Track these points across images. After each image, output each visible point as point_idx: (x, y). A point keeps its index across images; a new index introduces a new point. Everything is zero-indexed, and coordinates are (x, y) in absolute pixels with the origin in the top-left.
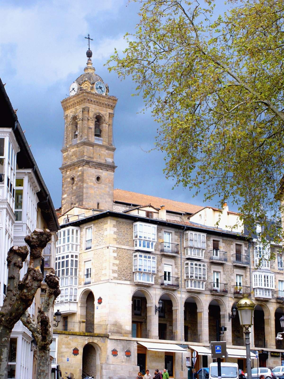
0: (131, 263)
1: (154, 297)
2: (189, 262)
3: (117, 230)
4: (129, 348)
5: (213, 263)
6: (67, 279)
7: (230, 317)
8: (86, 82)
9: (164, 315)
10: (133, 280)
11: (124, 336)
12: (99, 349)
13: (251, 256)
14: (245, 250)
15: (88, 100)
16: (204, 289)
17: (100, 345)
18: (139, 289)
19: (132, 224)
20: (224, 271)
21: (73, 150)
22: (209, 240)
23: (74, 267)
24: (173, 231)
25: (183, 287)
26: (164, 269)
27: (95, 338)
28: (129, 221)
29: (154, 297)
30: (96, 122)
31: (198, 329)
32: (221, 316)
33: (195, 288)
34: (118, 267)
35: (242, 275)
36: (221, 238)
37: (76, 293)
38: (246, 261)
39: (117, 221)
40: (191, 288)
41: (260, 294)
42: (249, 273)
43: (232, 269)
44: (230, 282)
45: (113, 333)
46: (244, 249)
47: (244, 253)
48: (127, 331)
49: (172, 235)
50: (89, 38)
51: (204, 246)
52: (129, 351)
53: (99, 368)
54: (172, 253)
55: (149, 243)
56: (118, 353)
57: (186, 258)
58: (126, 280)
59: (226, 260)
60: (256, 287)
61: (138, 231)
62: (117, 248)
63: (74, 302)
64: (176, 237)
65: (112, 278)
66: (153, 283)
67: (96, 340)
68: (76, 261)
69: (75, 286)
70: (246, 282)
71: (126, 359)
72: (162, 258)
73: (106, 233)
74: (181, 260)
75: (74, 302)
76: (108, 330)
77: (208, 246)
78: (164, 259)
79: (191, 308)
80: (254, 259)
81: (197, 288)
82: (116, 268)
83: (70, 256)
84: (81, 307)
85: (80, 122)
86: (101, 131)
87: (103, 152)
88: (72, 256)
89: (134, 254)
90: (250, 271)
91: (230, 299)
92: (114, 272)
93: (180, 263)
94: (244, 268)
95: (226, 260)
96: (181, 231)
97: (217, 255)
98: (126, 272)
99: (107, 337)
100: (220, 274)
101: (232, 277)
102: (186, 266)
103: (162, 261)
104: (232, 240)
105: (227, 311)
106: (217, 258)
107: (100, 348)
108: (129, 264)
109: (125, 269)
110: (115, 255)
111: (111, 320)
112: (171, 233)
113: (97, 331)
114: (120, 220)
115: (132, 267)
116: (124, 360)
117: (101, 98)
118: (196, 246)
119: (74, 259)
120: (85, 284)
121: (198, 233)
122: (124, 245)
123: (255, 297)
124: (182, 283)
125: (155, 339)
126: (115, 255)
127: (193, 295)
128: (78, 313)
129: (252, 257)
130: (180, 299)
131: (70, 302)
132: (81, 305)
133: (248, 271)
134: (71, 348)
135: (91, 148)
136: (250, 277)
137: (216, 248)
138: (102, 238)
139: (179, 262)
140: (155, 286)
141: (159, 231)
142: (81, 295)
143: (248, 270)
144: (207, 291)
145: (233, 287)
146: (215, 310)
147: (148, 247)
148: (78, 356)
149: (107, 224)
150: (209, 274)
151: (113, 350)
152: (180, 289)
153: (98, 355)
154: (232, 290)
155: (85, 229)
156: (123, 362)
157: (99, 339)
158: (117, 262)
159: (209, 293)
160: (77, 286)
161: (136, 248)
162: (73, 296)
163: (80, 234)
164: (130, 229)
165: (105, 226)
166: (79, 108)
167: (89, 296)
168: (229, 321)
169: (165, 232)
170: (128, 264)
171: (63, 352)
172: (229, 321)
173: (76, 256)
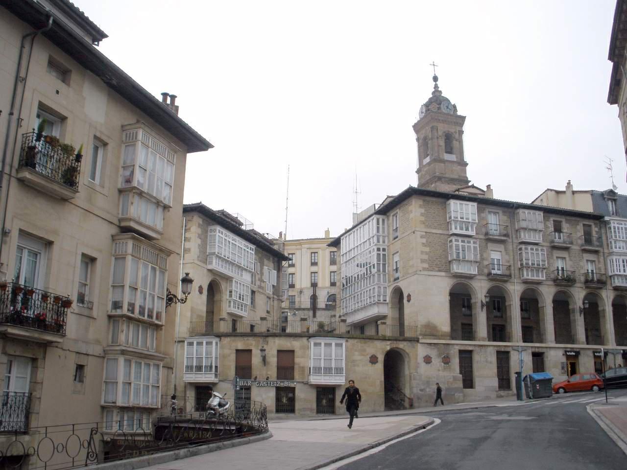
0: (445, 251)
1: (480, 290)
2: (523, 247)
3: (425, 211)
4: (448, 354)
5: (554, 248)
7: (581, 312)
9: (502, 315)
10: (450, 271)
11: (440, 339)
12: (407, 356)
13: (604, 238)
14: (596, 231)
15: (436, 119)
16: (544, 278)
17: (407, 351)
19: (445, 202)
20: (569, 256)
21: (425, 169)
22: (548, 221)
24: (500, 211)
25: (517, 277)
26: (490, 256)
27: (400, 342)
28: (440, 200)
29: (480, 290)
30: (445, 140)
32: (571, 311)
33: (533, 278)
34: (429, 256)
35: (594, 261)
36: (563, 217)
37: (385, 292)
38: (598, 244)
39: (424, 201)
40: (527, 278)
41: (619, 282)
42: (602, 258)
43: (581, 254)
44: (579, 269)
45: (425, 335)
46: (594, 230)
47: (594, 234)
48: (445, 332)
49: (499, 215)
50: (434, 65)
51: (541, 226)
52: (448, 357)
53: (407, 378)
54: (500, 236)
55: (467, 225)
56: (433, 360)
57: (519, 243)
58: (440, 271)
59: (572, 243)
60: (613, 274)
61: (452, 210)
62: (426, 232)
63: (383, 303)
64: (505, 218)
65: (421, 269)
66: (476, 273)
67: (402, 345)
68: (384, 255)
70: (600, 269)
72: (487, 244)
73: (412, 216)
74: (512, 244)
75: (383, 303)
76: (419, 332)
77: (546, 227)
78: (490, 245)
79: (530, 303)
80: (608, 242)
81: (535, 278)
82: (426, 257)
83: (376, 250)
84: (391, 308)
85: (430, 142)
86: (452, 149)
87: (454, 168)
88: (378, 249)
89: (449, 239)
91: (580, 290)
92: (423, 261)
93: (511, 249)
94: (596, 252)
95: (572, 243)
96: (510, 210)
97: (560, 238)
99: (418, 341)
100: (566, 261)
101: (581, 264)
102: (520, 252)
103: (487, 247)
104: (578, 219)
105: (577, 304)
106: (559, 240)
107: (408, 354)
108: (443, 251)
110: (424, 241)
111: (422, 320)
112: (498, 213)
113: (408, 334)
114: (428, 198)
117: (449, 117)
118: (530, 227)
119: (381, 253)
120: (395, 280)
121: (532, 212)
122: (436, 229)
123: (613, 285)
124: (514, 271)
126: (424, 241)
127: (531, 286)
128: (389, 316)
129: (605, 238)
130: (515, 291)
131: (378, 303)
133: (601, 256)
134: (367, 355)
135: (443, 164)
136: (605, 262)
137: (558, 229)
139: (510, 247)
140: (478, 277)
141: (480, 211)
143: (601, 254)
144: (549, 281)
145: (583, 275)
146: (562, 305)
147: (467, 229)
149: (411, 204)
150: (551, 261)
151: (426, 356)
152: (512, 280)
153: (406, 363)
154: (583, 279)
156: (439, 370)
157: (405, 343)
158: (427, 249)
159: (551, 283)
160: (386, 284)
161: (451, 232)
162: (382, 297)
164: (443, 209)
165: (410, 208)
166: (428, 128)
167: (399, 296)
168: (580, 316)
170: (441, 251)
172: (580, 316)
173: (384, 250)
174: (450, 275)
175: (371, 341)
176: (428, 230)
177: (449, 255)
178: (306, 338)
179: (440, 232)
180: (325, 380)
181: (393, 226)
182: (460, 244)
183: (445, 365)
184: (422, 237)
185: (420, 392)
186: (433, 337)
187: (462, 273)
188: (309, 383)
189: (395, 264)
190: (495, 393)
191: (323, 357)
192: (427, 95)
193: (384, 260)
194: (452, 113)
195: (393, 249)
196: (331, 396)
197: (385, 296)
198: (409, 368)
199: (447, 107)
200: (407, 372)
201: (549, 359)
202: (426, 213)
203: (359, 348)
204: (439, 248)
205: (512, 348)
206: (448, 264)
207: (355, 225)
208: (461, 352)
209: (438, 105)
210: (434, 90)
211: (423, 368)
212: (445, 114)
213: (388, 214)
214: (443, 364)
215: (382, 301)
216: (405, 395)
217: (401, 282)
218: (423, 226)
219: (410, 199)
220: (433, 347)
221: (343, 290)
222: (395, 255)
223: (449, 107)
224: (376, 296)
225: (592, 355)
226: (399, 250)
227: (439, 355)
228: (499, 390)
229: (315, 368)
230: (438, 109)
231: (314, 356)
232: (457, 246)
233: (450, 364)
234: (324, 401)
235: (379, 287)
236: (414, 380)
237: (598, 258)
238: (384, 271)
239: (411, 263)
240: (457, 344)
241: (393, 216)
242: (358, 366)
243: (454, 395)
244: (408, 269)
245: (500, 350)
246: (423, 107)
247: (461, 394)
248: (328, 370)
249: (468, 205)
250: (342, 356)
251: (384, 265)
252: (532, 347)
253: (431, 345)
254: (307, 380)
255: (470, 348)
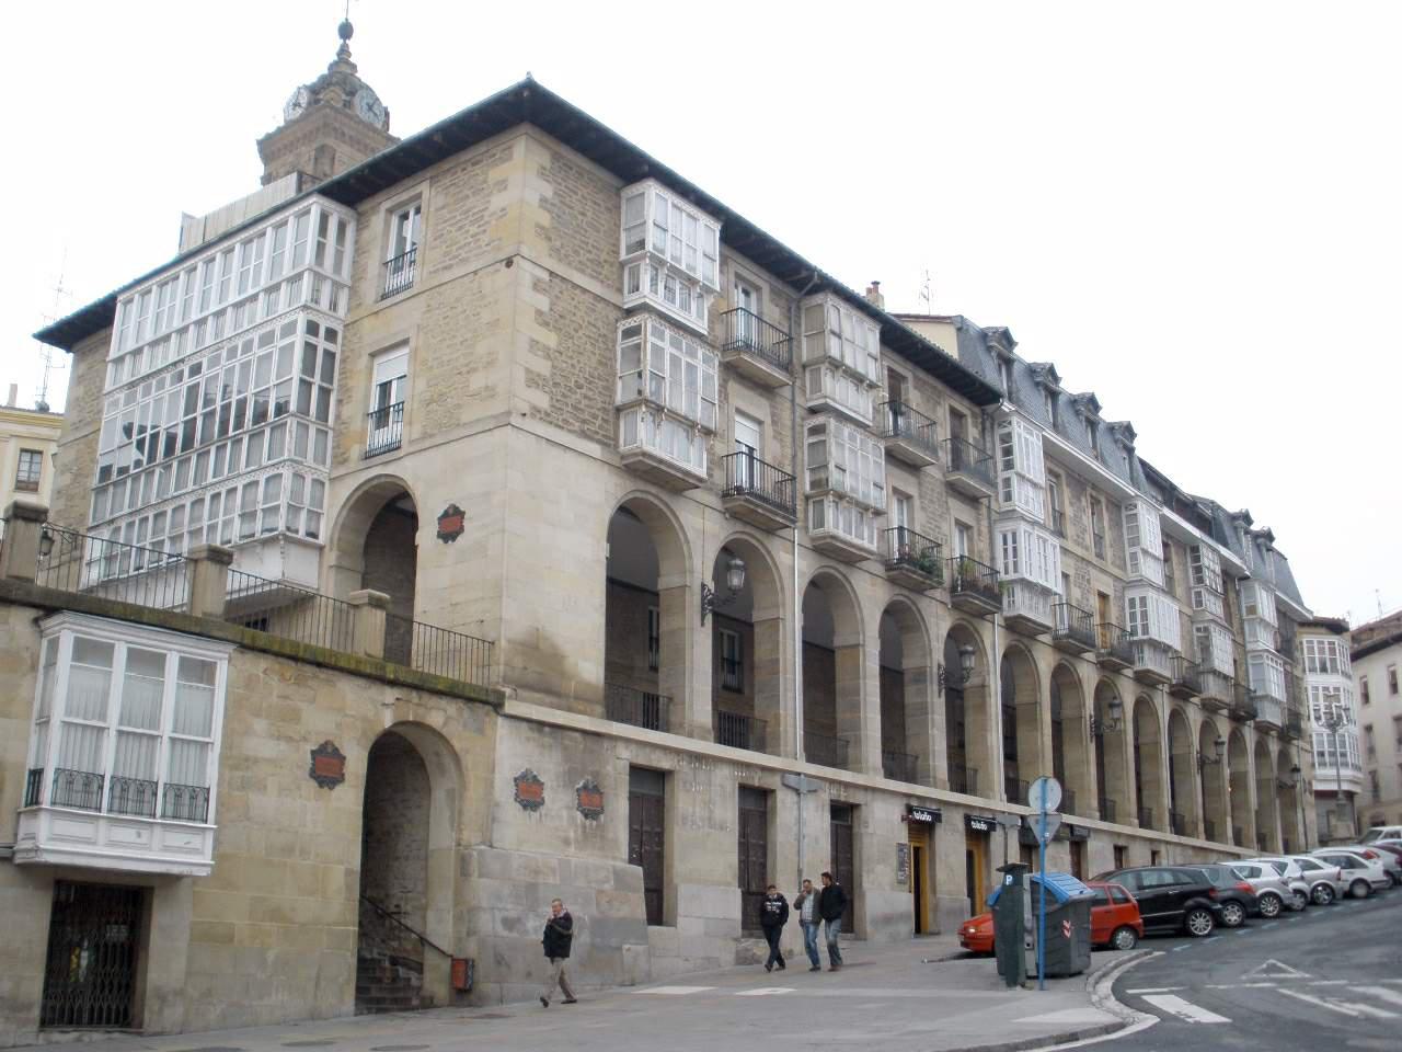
4: (596, 775)
6: (277, 433)
8: (332, 88)
10: (616, 446)
11: (570, 709)
15: (335, 129)
17: (457, 745)
18: (639, 495)
19: (618, 195)
23: (317, 380)
27: (433, 701)
31: (840, 716)
34: (554, 367)
39: (556, 157)
43: (944, 494)
48: (588, 684)
53: (444, 868)
56: (546, 794)
58: (584, 435)
60: (1012, 576)
62: (551, 273)
65: (526, 409)
67: (440, 714)
68: (330, 355)
69: (314, 465)
71: (584, 827)
73: (498, 201)
82: (543, 367)
83: (301, 327)
84: (339, 567)
88: (312, 328)
90: (989, 518)
91: (940, 610)
92: (534, 380)
93: (789, 423)
98: (586, 397)
99: (496, 704)
102: (813, 440)
108: (600, 363)
109: (582, 381)
110: (543, 302)
115: (614, 383)
116: (572, 835)
117: (371, 134)
119: (321, 343)
120: (368, 456)
122: (583, 272)
125: (704, 738)
126: (543, 302)
131: (288, 539)
132: (339, 558)
134: (305, 739)
138: (473, 230)
142: (344, 513)
148: (339, 789)
153: (439, 795)
155: (382, 214)
156: (567, 842)
157: (452, 707)
158: (550, 339)
161: (631, 301)
162: (303, 515)
163: (356, 242)
164: (608, 209)
169: (738, 276)
170: (594, 360)
171: (256, 761)
173: (331, 335)
174: (616, 461)
175: (323, 674)
176: (561, 269)
177: (619, 384)
178: (31, 613)
179: (595, 287)
180: (112, 844)
181: (385, 248)
182: (669, 350)
183: (588, 822)
184: (537, 286)
185: (505, 933)
186: (548, 699)
187: (661, 461)
188: (18, 859)
189: (375, 393)
190: (733, 946)
191: (113, 722)
192: (315, 67)
193: (328, 375)
194: (379, 126)
195: (374, 332)
196: (117, 933)
197: (315, 515)
198: (457, 822)
199: (370, 108)
200: (441, 836)
201: (870, 830)
202: (556, 201)
203: (274, 699)
204: (588, 346)
205: (783, 777)
206: (611, 417)
207: (185, 250)
208: (636, 771)
209: (347, 95)
210: (336, 58)
211: (513, 824)
212: (361, 122)
213: (365, 206)
214: (579, 815)
215: (301, 535)
216: (423, 940)
217: (407, 462)
218: (543, 246)
219: (503, 138)
220: (547, 740)
221: (100, 491)
222: (378, 361)
223: (375, 108)
224: (283, 511)
225: (961, 826)
226: (411, 334)
227: (570, 776)
228: (743, 936)
229: (66, 777)
230: (345, 105)
231: (68, 712)
232: (658, 351)
233: (602, 817)
234: (84, 958)
235: (298, 476)
236: (480, 876)
237: (978, 521)
238: (323, 414)
239: (477, 382)
240: (628, 741)
241: (390, 211)
242: (262, 788)
243: (619, 949)
244: (459, 406)
245: (750, 782)
246: (302, 91)
247: (640, 948)
248: (133, 796)
249: (695, 219)
250: (208, 731)
251: (325, 393)
252: (832, 782)
253: (540, 731)
254: (8, 840)
255: (664, 763)
